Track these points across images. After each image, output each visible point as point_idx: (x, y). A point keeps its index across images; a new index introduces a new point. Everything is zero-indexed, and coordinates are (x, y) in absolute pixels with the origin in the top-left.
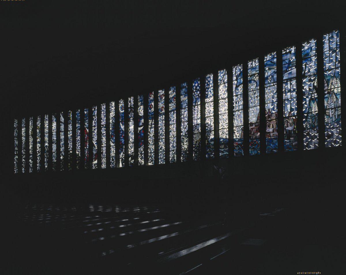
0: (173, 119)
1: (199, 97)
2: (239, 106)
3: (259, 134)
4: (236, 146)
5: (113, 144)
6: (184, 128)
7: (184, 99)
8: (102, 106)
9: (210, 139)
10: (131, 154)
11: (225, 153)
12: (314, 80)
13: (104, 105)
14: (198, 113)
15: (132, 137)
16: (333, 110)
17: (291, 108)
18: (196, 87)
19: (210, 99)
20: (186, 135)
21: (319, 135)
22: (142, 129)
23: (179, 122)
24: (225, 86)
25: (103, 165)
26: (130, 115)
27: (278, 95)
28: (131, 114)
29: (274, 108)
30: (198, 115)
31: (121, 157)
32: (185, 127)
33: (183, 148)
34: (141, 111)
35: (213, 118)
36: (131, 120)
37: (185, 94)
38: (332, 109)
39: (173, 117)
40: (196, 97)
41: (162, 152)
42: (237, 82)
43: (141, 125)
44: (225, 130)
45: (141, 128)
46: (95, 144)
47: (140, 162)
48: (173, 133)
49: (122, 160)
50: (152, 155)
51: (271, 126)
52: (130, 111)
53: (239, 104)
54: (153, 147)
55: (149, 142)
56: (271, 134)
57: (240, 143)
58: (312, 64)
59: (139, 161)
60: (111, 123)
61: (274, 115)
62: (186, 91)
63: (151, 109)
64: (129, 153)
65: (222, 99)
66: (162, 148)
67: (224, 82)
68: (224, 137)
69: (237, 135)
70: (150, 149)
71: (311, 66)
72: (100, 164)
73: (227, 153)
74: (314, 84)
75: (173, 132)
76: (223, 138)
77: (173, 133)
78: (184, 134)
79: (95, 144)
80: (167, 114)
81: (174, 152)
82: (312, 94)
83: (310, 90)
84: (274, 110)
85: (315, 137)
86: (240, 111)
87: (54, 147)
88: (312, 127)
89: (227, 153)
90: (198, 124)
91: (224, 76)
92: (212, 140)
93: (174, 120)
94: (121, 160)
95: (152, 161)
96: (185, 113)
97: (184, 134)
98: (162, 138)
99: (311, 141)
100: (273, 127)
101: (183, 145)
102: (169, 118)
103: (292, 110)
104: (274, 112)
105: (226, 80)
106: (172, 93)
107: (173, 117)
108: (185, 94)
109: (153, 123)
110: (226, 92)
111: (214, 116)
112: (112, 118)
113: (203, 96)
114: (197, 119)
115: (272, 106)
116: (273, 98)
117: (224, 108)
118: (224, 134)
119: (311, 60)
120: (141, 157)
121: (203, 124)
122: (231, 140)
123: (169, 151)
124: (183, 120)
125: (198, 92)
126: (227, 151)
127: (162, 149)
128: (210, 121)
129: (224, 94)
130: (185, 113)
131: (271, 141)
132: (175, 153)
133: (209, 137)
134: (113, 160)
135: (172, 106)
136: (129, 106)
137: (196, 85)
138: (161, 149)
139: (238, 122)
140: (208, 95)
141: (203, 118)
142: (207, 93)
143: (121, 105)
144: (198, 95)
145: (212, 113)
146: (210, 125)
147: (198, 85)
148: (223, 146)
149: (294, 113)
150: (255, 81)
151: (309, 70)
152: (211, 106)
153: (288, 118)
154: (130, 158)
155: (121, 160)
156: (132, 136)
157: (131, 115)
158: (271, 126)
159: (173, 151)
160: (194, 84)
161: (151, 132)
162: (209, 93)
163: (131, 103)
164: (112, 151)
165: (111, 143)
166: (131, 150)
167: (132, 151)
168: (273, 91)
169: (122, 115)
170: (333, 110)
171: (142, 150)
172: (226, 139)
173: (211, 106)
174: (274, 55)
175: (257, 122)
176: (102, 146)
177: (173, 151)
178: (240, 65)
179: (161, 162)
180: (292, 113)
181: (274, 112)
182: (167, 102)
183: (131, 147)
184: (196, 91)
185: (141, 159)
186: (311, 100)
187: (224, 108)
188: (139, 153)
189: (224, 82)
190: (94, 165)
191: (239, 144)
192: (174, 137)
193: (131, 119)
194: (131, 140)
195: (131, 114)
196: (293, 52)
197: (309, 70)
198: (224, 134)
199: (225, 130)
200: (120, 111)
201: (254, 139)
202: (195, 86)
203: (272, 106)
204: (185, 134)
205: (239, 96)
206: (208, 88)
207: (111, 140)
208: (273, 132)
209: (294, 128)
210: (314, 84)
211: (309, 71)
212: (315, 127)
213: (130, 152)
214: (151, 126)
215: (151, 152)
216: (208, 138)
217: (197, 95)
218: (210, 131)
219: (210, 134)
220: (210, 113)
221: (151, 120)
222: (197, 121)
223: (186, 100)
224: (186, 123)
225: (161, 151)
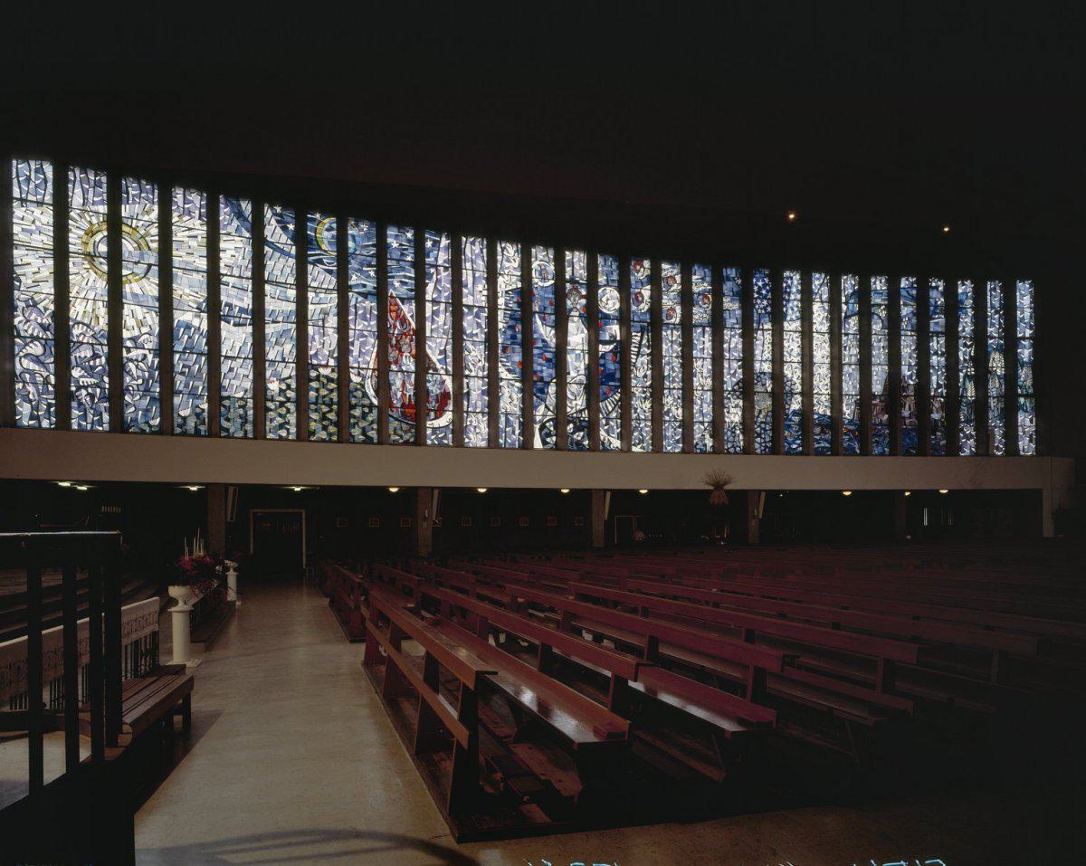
0: (701, 347)
1: (766, 313)
2: (851, 356)
3: (886, 416)
4: (846, 434)
5: (510, 376)
6: (729, 374)
7: (731, 306)
8: (468, 245)
9: (791, 411)
10: (575, 415)
11: (823, 445)
12: (971, 346)
13: (473, 243)
14: (763, 346)
15: (577, 367)
16: (995, 400)
17: (938, 383)
18: (760, 288)
19: (792, 325)
20: (734, 390)
21: (976, 434)
22: (611, 351)
23: (718, 358)
24: (824, 307)
25: (471, 436)
26: (569, 302)
27: (918, 354)
28: (575, 300)
29: (911, 376)
30: (763, 352)
31: (538, 418)
32: (732, 372)
33: (727, 420)
34: (610, 301)
35: (786, 324)
36: (576, 319)
37: (734, 295)
38: (994, 398)
39: (703, 342)
40: (759, 311)
41: (669, 421)
42: (848, 308)
43: (607, 338)
44: (823, 398)
45: (607, 347)
46: (437, 364)
47: (604, 439)
48: (702, 380)
49: (543, 427)
50: (641, 426)
51: (907, 406)
52: (571, 290)
53: (851, 353)
54: (648, 405)
55: (634, 390)
56: (907, 421)
57: (851, 427)
58: (968, 320)
59: (602, 438)
60: (503, 307)
61: (912, 388)
62: (735, 290)
63: (639, 302)
64: (568, 409)
65: (817, 332)
66: (669, 411)
67: (821, 298)
68: (821, 412)
69: (848, 411)
70: (636, 409)
71: (966, 323)
72: (458, 429)
73: (827, 445)
74: (970, 352)
75: (701, 379)
76: (818, 414)
77: (702, 380)
78: (730, 389)
79: (437, 364)
80: (687, 326)
81: (702, 427)
82: (968, 367)
83: (965, 360)
84: (911, 379)
85: (972, 436)
86: (853, 367)
87: (235, 338)
88: (968, 421)
89: (827, 445)
90: (764, 374)
91: (821, 285)
92: (795, 413)
93: (703, 349)
94: (537, 427)
95: (642, 441)
96: (733, 341)
97: (730, 389)
98: (672, 387)
99: (966, 442)
100: (910, 409)
101: (728, 412)
102: (691, 340)
103: (939, 386)
104: (912, 383)
105: (825, 297)
106: (699, 283)
107: (703, 342)
108: (734, 295)
109: (644, 342)
110: (825, 321)
111: (802, 363)
112: (507, 292)
113: (778, 317)
114: (762, 361)
115: (909, 371)
116: (910, 358)
117: (821, 352)
118: (822, 407)
119: (966, 314)
120: (606, 428)
121: (777, 376)
122: (834, 423)
123: (692, 424)
124: (727, 354)
125: (765, 302)
126: (826, 440)
127: (671, 415)
128: (793, 372)
129: (821, 323)
130: (733, 341)
131: (906, 433)
132: (705, 429)
133: (790, 405)
134: (508, 423)
135: (700, 314)
136: (567, 277)
137: (760, 284)
138: (668, 415)
139: (850, 386)
140: (786, 316)
141: (778, 359)
142: (785, 309)
143: (538, 262)
144: (765, 308)
145: (795, 355)
146: (791, 380)
147: (765, 285)
148: (818, 430)
149: (942, 392)
150: (880, 317)
151: (964, 327)
152: (793, 340)
153: (934, 397)
154: (571, 425)
155: (537, 427)
156: (577, 364)
157: (576, 303)
158: (907, 406)
159: (702, 423)
160: (754, 280)
161: (639, 365)
162: (790, 311)
163: (573, 266)
164: (507, 395)
165: (500, 370)
166: (577, 402)
167: (578, 407)
168: (911, 346)
169: (542, 293)
170: (995, 400)
171: (610, 409)
172: (824, 415)
173: (793, 340)
174: (913, 283)
175: (882, 395)
176: (467, 372)
177: (702, 423)
178: (854, 276)
179: (669, 448)
180: (939, 391)
181: (912, 383)
182: (687, 298)
183: (573, 393)
184: (758, 298)
185: (607, 432)
186: (966, 376)
187: (821, 352)
188: (601, 416)
189: (821, 298)
190: (434, 433)
191: (850, 431)
192: (703, 389)
193: (573, 313)
194: (573, 374)
195: (575, 300)
196: (940, 288)
197: (964, 327)
198: (822, 407)
199: (823, 398)
200: (536, 280)
201: (878, 425)
202: (757, 285)
203: (909, 371)
204: (733, 387)
205: (851, 337)
206: (788, 301)
207: (501, 361)
208: (910, 417)
209: (942, 417)
210: (970, 352)
211: (964, 331)
212: (971, 421)
213: (572, 408)
214: (639, 348)
215: (638, 419)
216: (787, 407)
217: (762, 306)
218: (792, 394)
219: (791, 400)
220: (790, 355)
221: (639, 334)
222: (763, 365)
223: (734, 310)
224: (735, 365)
225: (667, 418)
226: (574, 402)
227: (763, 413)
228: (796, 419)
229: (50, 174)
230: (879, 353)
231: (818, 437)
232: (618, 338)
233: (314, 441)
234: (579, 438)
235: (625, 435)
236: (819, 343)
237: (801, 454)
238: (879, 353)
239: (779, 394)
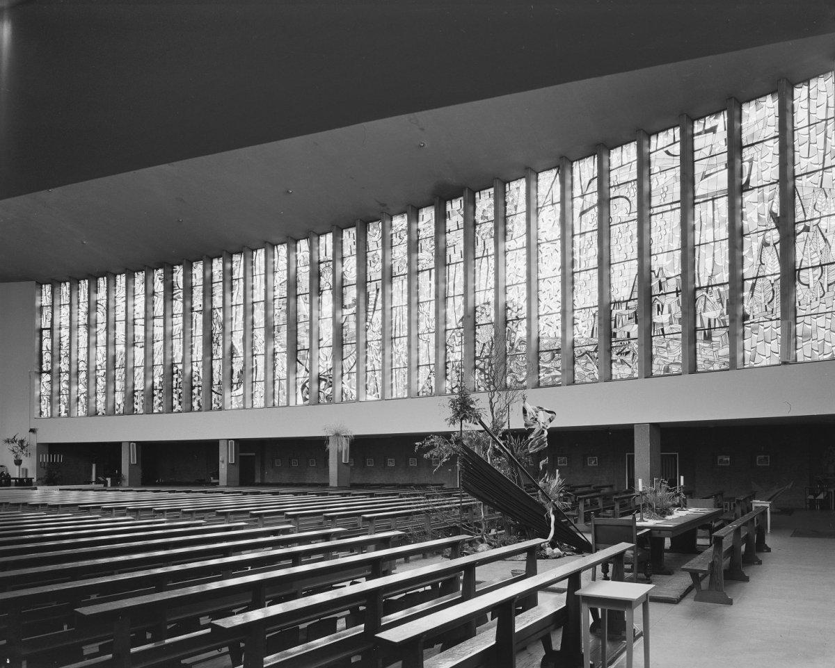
10: (326, 374)
53: (586, 253)
107: (426, 284)
118: (550, 330)
139: (586, 294)
209: (722, 314)
222: (667, 264)
226: (326, 363)
227: (487, 347)
228: (523, 348)
229: (87, 283)
230: (624, 244)
231: (547, 365)
232: (778, 215)
233: (175, 412)
234: (329, 393)
235: (362, 385)
236: (549, 254)
237: (327, 404)
238: (624, 244)
239: (503, 323)
